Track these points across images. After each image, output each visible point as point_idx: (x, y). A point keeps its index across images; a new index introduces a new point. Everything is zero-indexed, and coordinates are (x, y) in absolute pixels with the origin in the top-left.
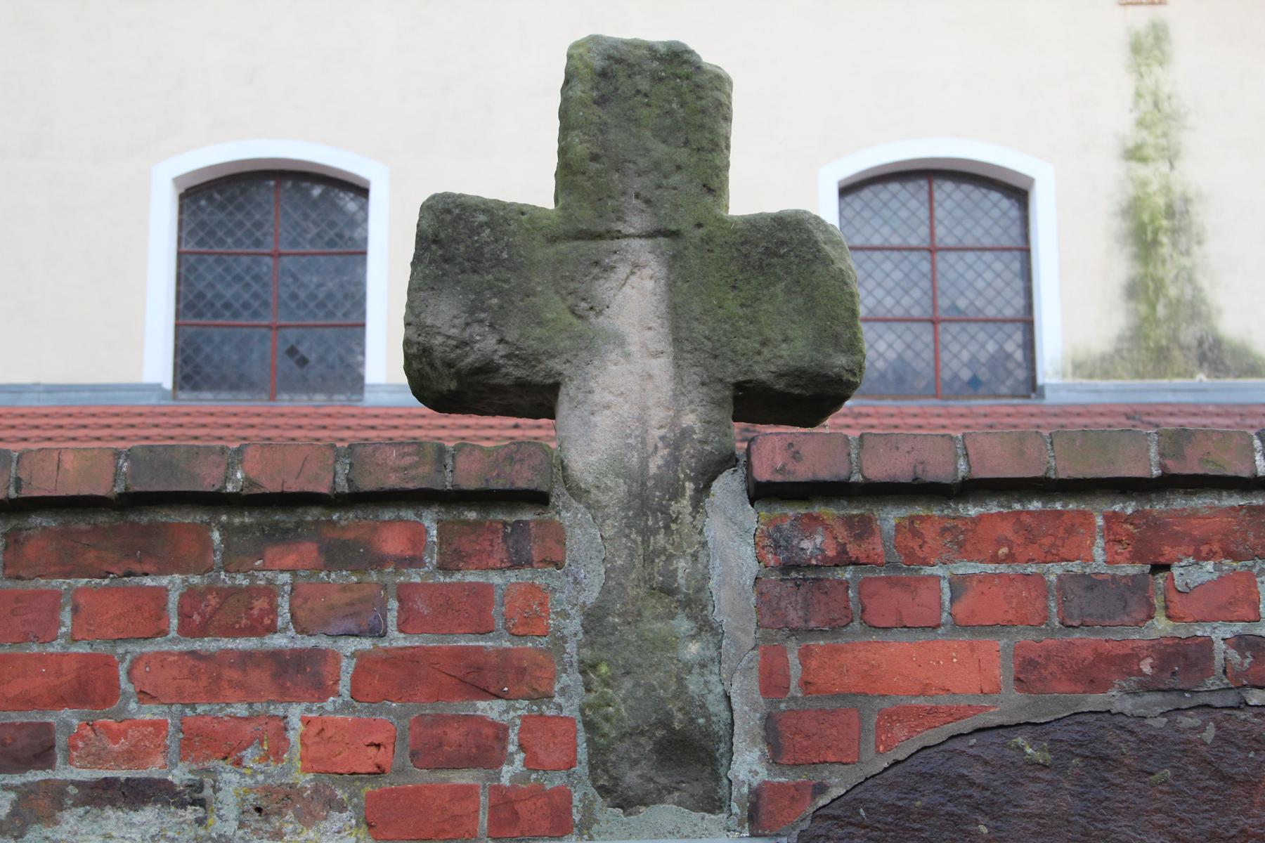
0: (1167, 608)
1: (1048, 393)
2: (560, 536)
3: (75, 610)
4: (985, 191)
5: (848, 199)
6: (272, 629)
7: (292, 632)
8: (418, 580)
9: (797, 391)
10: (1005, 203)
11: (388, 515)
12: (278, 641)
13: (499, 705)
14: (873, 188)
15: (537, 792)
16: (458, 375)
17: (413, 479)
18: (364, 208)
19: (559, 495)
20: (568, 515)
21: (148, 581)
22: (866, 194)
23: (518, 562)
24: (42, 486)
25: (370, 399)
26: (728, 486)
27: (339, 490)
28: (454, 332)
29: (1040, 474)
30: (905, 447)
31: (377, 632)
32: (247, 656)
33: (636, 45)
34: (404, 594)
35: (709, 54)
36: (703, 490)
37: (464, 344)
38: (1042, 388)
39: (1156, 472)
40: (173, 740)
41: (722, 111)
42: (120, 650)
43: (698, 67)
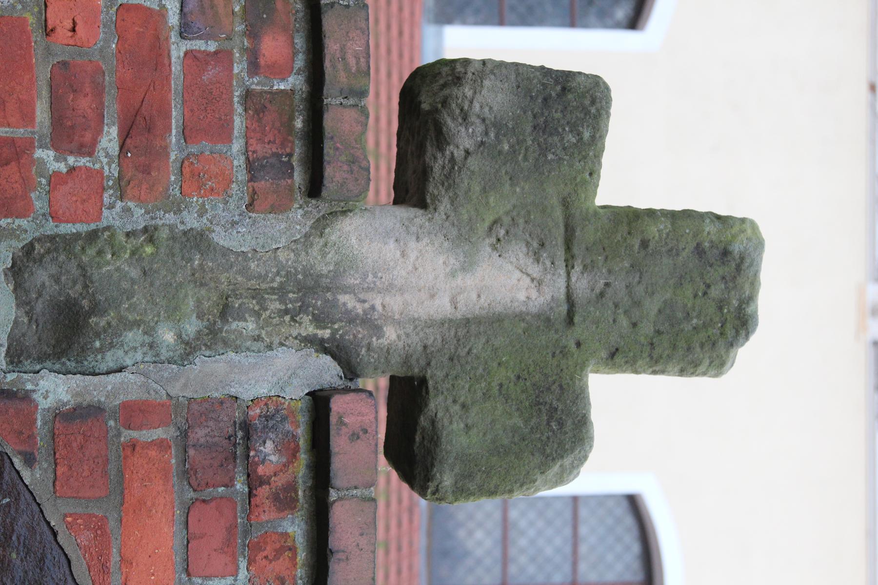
2: (278, 208)
5: (625, 504)
8: (236, 70)
9: (418, 438)
11: (300, 41)
15: (27, 184)
17: (334, 67)
22: (629, 521)
23: (253, 168)
28: (477, 106)
30: (363, 542)
33: (754, 283)
34: (222, 57)
36: (322, 347)
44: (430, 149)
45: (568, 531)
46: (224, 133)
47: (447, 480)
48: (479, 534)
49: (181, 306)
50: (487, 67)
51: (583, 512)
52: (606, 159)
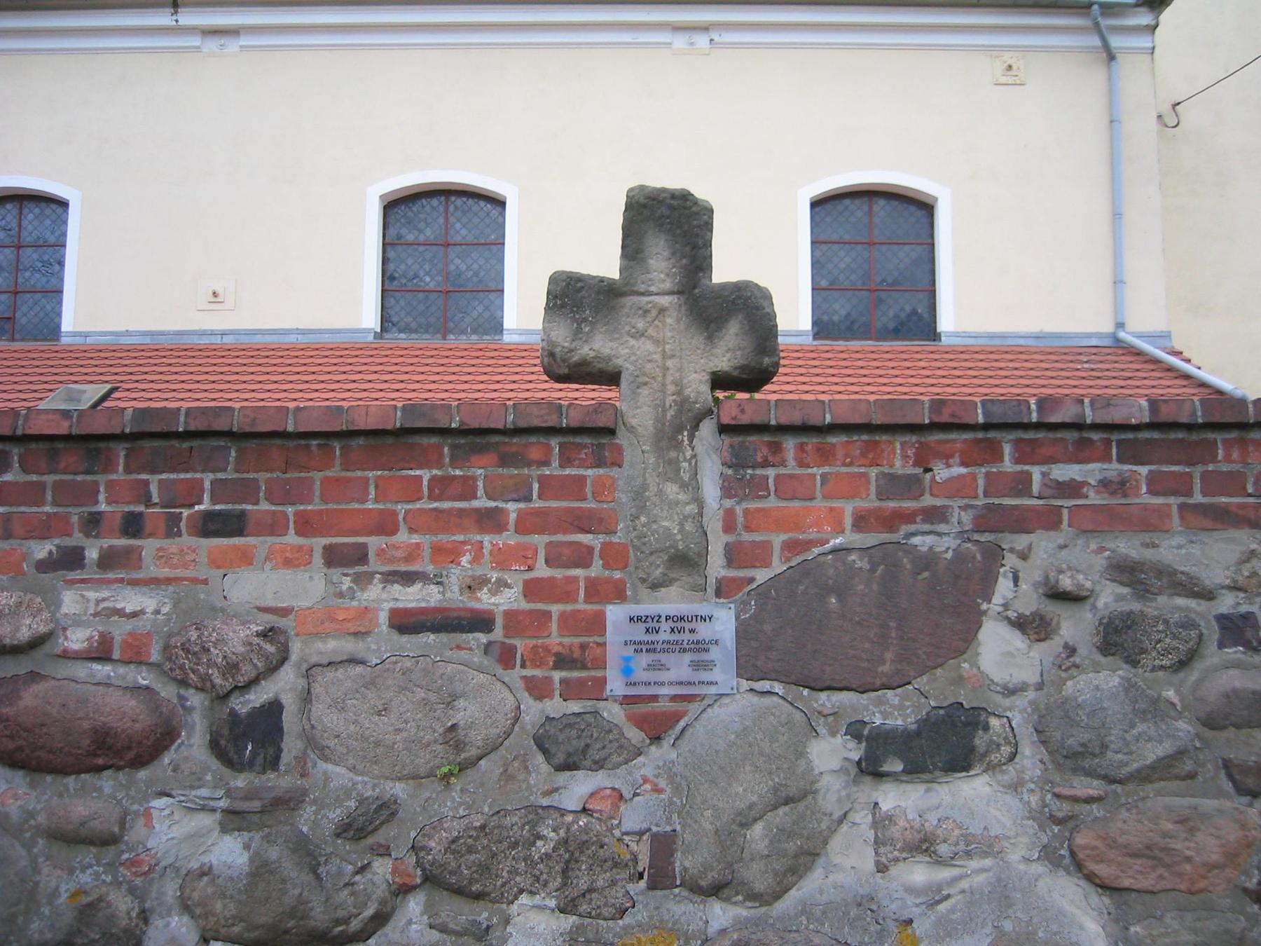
0: (931, 490)
1: (943, 339)
2: (619, 449)
3: (377, 487)
4: (906, 205)
5: (817, 209)
6: (475, 497)
7: (485, 499)
8: (548, 473)
9: (744, 376)
10: (920, 213)
11: (533, 439)
12: (476, 504)
13: (590, 536)
14: (832, 202)
15: (608, 580)
16: (569, 367)
17: (546, 421)
18: (503, 214)
19: (622, 431)
20: (622, 439)
21: (412, 473)
22: (829, 206)
23: (599, 464)
24: (361, 425)
25: (507, 338)
26: (707, 429)
27: (508, 426)
28: (566, 344)
29: (867, 421)
30: (798, 407)
31: (528, 499)
32: (461, 511)
33: (664, 190)
34: (542, 480)
35: (700, 192)
36: (696, 427)
37: (571, 351)
38: (940, 333)
39: (927, 421)
40: (427, 553)
41: (709, 226)
42: (399, 507)
43: (696, 202)
44: (589, 369)
45: (835, 247)
46: (583, 479)
47: (767, 360)
48: (837, 306)
49: (992, 834)
50: (896, 824)
51: (823, 237)
52: (594, 274)
